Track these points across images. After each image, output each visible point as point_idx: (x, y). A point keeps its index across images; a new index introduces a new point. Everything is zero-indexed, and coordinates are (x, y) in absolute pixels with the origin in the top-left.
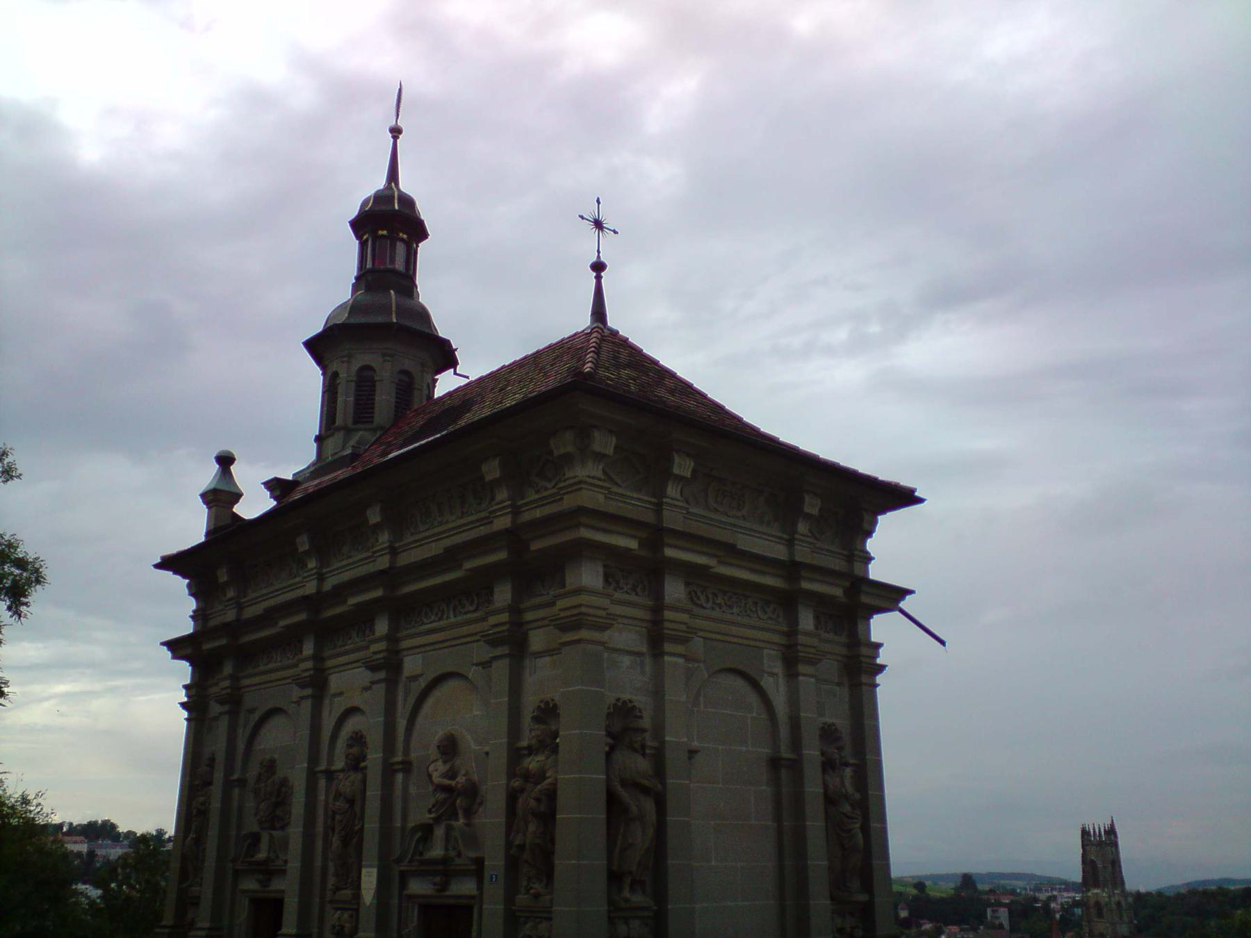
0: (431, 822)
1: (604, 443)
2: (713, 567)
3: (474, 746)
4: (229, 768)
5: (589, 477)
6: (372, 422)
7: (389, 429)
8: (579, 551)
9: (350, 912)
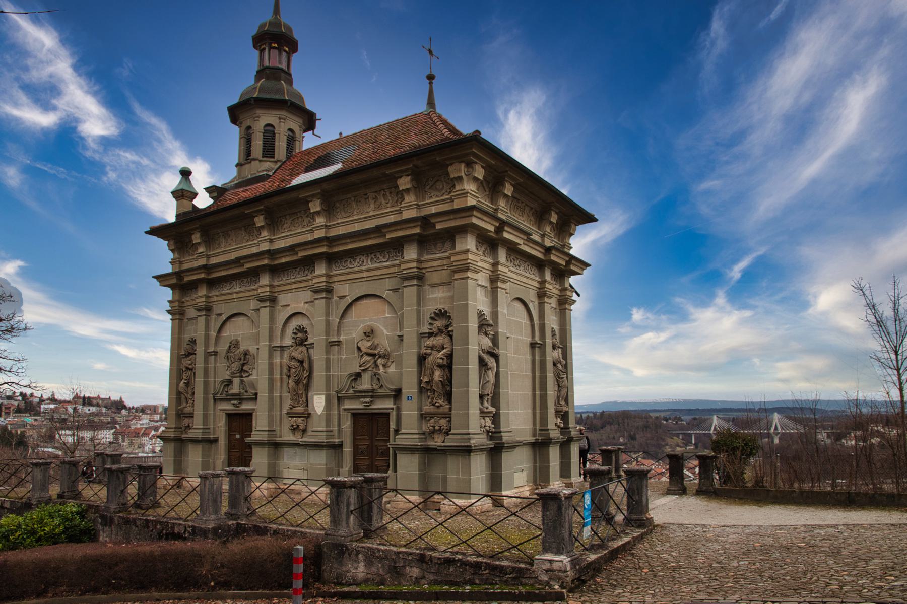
0: (360, 371)
1: (479, 173)
2: (520, 245)
3: (385, 332)
4: (207, 345)
5: (471, 190)
6: (274, 157)
7: (285, 161)
8: (463, 230)
9: (303, 418)
